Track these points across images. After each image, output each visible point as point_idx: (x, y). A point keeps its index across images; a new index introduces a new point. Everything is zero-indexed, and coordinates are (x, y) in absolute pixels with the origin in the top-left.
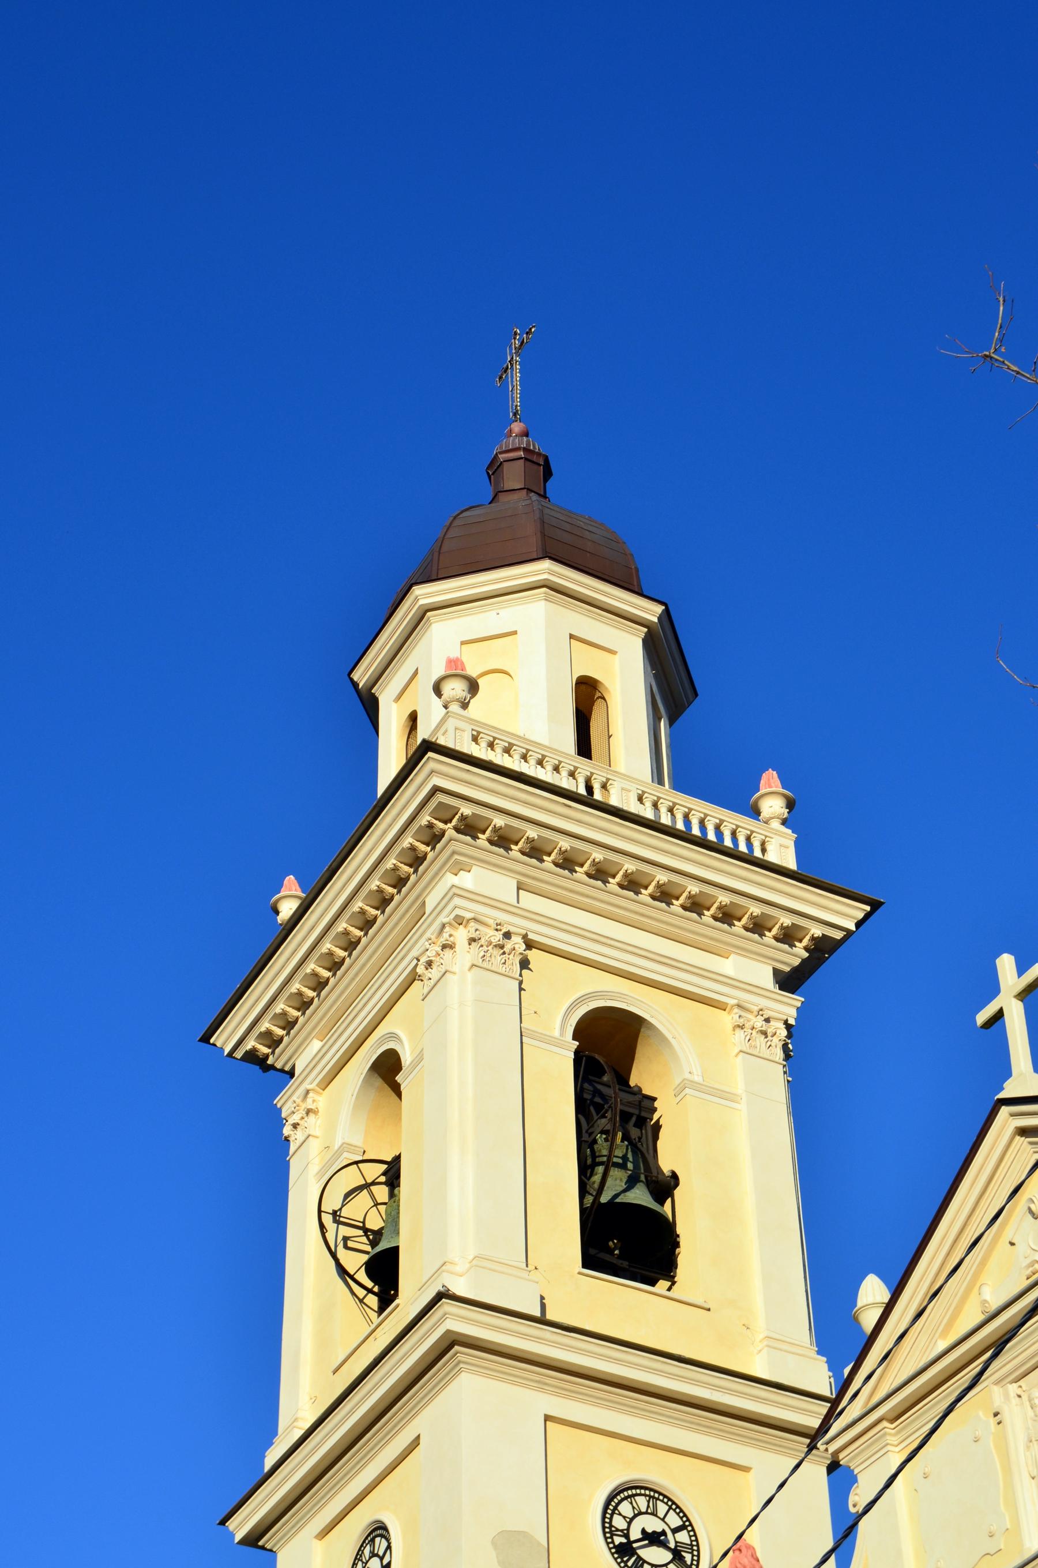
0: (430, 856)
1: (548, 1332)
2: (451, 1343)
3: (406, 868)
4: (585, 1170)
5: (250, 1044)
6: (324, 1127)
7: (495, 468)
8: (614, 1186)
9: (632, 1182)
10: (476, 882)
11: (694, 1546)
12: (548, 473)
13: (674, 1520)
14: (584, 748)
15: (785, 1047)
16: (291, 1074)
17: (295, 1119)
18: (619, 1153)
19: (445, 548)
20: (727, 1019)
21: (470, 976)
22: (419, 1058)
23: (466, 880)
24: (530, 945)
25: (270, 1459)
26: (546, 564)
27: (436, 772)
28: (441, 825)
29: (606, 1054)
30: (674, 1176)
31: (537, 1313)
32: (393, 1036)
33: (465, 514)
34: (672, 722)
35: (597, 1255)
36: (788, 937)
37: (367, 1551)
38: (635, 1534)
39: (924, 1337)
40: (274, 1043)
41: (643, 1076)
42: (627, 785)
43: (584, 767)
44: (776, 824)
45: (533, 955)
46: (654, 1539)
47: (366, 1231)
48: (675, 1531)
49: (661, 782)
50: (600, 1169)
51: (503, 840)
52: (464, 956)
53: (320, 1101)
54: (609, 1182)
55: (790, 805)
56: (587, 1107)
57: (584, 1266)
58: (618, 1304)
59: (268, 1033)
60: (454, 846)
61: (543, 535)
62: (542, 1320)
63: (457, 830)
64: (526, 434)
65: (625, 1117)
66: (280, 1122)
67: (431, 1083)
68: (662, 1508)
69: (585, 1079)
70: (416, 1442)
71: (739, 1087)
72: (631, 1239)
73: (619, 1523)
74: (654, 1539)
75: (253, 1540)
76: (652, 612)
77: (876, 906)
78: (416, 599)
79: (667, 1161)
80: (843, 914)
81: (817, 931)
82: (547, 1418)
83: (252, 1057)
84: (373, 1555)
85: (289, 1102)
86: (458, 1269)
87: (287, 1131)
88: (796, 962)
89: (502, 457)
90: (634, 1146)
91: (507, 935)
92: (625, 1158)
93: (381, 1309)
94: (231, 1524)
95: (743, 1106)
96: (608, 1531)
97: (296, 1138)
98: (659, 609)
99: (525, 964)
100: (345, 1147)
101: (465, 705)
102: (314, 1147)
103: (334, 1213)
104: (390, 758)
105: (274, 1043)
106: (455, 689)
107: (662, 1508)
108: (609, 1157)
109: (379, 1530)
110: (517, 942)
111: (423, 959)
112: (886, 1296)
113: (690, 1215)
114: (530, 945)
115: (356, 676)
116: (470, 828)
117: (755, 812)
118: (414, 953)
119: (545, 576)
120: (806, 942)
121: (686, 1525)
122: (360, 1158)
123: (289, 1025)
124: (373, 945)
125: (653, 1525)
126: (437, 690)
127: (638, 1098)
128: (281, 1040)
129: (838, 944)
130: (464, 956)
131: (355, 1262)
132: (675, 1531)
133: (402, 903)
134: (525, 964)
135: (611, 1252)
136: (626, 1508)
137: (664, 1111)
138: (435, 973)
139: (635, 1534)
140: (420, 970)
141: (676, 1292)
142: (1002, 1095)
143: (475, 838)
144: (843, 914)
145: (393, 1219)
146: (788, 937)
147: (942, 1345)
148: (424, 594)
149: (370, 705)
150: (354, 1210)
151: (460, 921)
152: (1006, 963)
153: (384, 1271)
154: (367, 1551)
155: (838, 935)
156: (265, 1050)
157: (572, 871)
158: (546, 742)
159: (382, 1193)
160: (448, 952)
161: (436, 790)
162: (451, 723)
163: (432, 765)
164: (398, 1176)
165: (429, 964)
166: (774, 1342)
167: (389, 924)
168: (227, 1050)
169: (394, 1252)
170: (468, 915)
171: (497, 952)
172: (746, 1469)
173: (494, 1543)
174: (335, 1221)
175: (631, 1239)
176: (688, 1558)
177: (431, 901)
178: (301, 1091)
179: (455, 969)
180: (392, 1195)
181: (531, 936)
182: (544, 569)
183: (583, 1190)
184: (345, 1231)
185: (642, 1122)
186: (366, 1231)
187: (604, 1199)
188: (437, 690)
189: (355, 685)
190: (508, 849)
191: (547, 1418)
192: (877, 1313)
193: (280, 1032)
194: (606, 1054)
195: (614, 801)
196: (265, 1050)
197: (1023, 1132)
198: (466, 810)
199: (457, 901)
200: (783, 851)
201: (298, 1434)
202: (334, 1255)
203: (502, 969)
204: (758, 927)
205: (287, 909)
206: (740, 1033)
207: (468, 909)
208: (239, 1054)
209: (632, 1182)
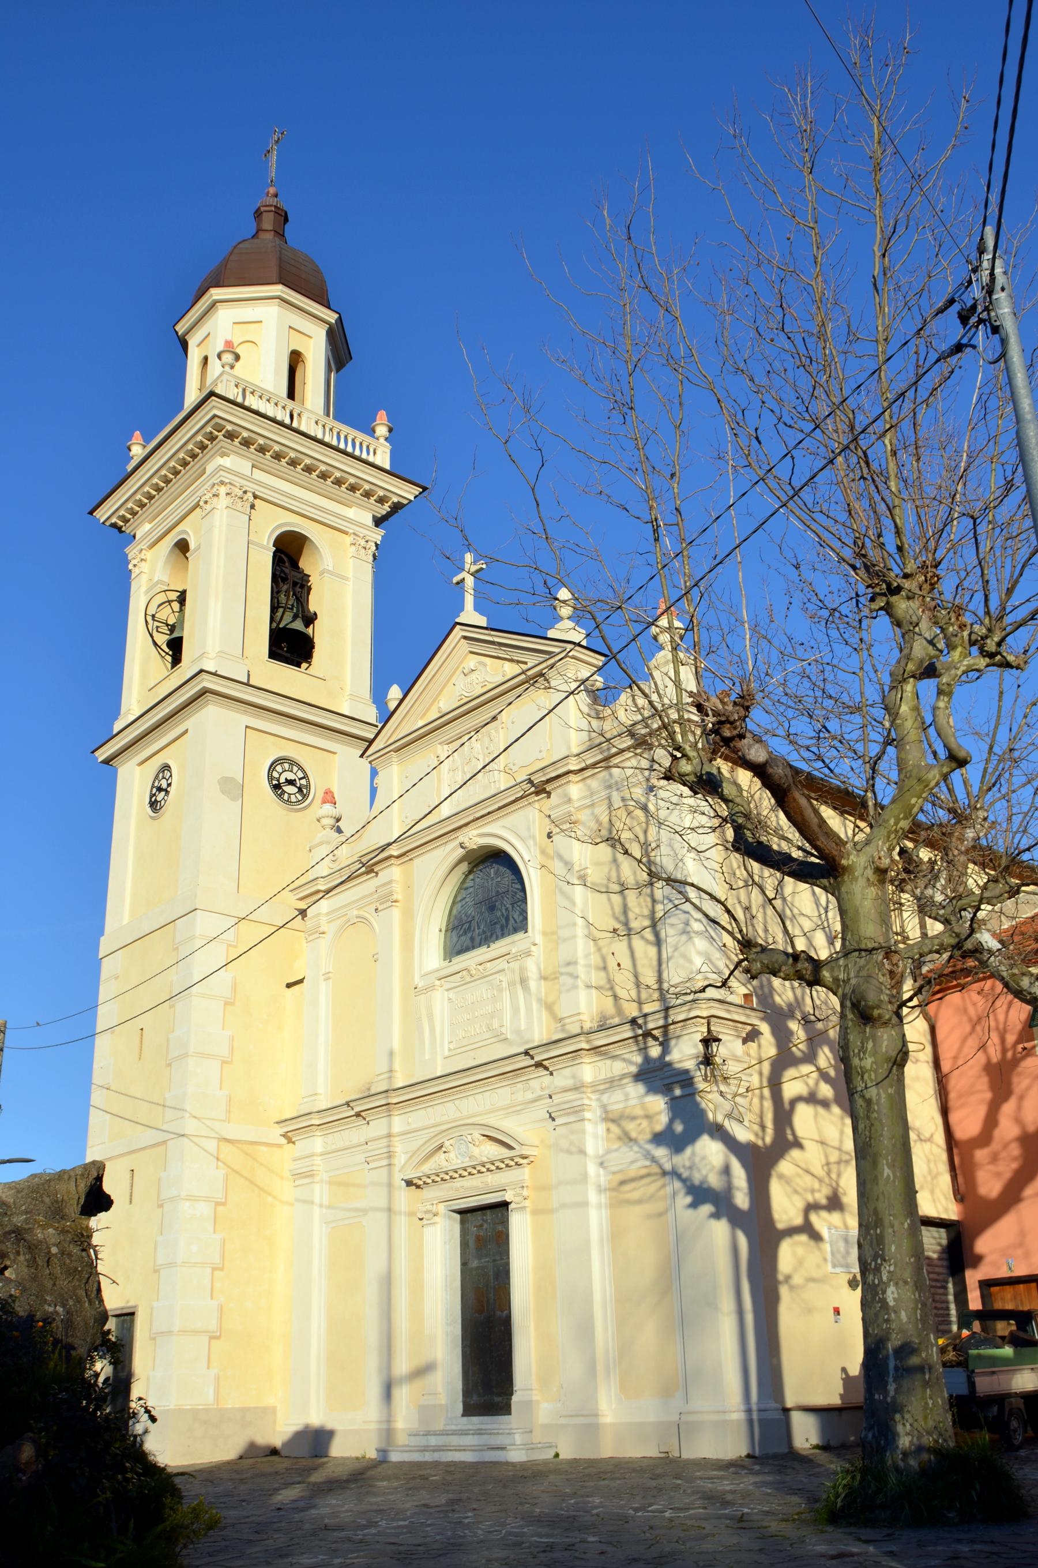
0: (210, 446)
1: (250, 689)
2: (204, 692)
3: (198, 450)
4: (274, 609)
5: (114, 520)
6: (149, 571)
7: (258, 214)
8: (287, 620)
9: (295, 617)
10: (230, 462)
11: (308, 786)
12: (286, 220)
13: (300, 774)
14: (291, 395)
15: (374, 556)
16: (134, 536)
17: (134, 562)
18: (290, 603)
19: (229, 266)
20: (348, 539)
21: (225, 511)
22: (198, 548)
23: (227, 462)
24: (255, 497)
25: (117, 728)
26: (280, 287)
27: (215, 408)
28: (216, 433)
29: (288, 555)
30: (315, 614)
31: (245, 681)
32: (185, 532)
33: (241, 246)
34: (338, 371)
35: (275, 654)
36: (381, 500)
37: (161, 775)
38: (282, 780)
39: (410, 719)
40: (126, 521)
41: (305, 564)
42: (311, 415)
43: (290, 404)
44: (382, 440)
45: (257, 502)
46: (291, 782)
47: (167, 625)
48: (300, 779)
49: (328, 415)
50: (281, 610)
51: (246, 443)
52: (223, 501)
53: (148, 555)
54: (285, 617)
55: (390, 430)
56: (277, 579)
57: (270, 657)
58: (283, 677)
59: (123, 516)
60: (222, 444)
61: (280, 267)
62: (248, 684)
63: (224, 436)
64: (276, 196)
65: (295, 584)
66: (128, 562)
67: (202, 556)
68: (295, 769)
69: (278, 565)
70: (186, 731)
71: (350, 574)
72: (291, 645)
73: (275, 775)
74: (291, 782)
75: (107, 762)
76: (332, 317)
77: (425, 489)
78: (211, 296)
79: (313, 607)
80: (407, 492)
81: (395, 499)
82: (247, 727)
83: (114, 525)
84: (164, 778)
85: (132, 551)
86: (211, 656)
87: (130, 567)
88: (384, 513)
89: (262, 209)
90: (298, 599)
91: (245, 492)
92: (293, 605)
93: (172, 668)
94: (97, 754)
95: (350, 583)
96: (270, 778)
97: (135, 572)
98: (336, 316)
99: (253, 507)
100: (159, 582)
101: (232, 367)
102: (144, 578)
103: (153, 616)
104: (192, 395)
105: (126, 521)
106: (228, 358)
107: (295, 769)
108: (286, 604)
109: (166, 767)
110: (250, 495)
111: (203, 499)
112: (401, 697)
113: (321, 633)
114: (255, 497)
115: (177, 328)
116: (230, 436)
117: (371, 432)
118: (199, 493)
119: (279, 293)
120: (389, 503)
121: (305, 777)
122: (166, 588)
123: (134, 514)
124: (177, 483)
125: (290, 776)
126: (219, 357)
127: (301, 575)
128: (129, 520)
129: (405, 505)
130: (223, 501)
131: (162, 639)
132: (300, 779)
133: (194, 466)
134: (253, 507)
135: (282, 649)
136: (279, 768)
137: (313, 581)
138: (208, 507)
139: (282, 780)
140: (201, 503)
141: (311, 671)
142: (457, 620)
143: (233, 440)
144: (407, 492)
145: (181, 620)
146: (381, 500)
147: (421, 723)
148: (216, 293)
149: (184, 345)
150: (162, 615)
151: (222, 483)
152: (469, 557)
153: (176, 646)
154: (161, 775)
155: (405, 502)
156: (121, 524)
157: (279, 461)
158: (271, 389)
159: (176, 606)
160: (216, 498)
161: (215, 416)
162: (225, 377)
163: (214, 403)
164: (184, 600)
165: (206, 502)
166: (353, 697)
167: (186, 474)
168: (102, 521)
169: (180, 640)
170: (227, 481)
171: (239, 501)
172: (335, 753)
173: (219, 782)
174: (154, 620)
175: (291, 645)
176: (305, 791)
177: (210, 468)
178: (138, 548)
179: (219, 507)
180: (181, 610)
181: (257, 493)
182: (278, 289)
183: (272, 620)
184: (156, 624)
185: (302, 586)
186: (167, 625)
187: (281, 626)
188: (219, 357)
189: (177, 333)
190: (248, 447)
191: (247, 727)
192: (396, 703)
193: (129, 516)
194: (288, 555)
195: (303, 428)
196: (121, 524)
197: (465, 638)
198: (229, 427)
199: (222, 473)
200: (383, 457)
201: (132, 718)
202: (152, 636)
203: (241, 509)
204: (367, 495)
205: (137, 451)
206: (353, 547)
207: (227, 478)
208: (108, 523)
209: (295, 617)
